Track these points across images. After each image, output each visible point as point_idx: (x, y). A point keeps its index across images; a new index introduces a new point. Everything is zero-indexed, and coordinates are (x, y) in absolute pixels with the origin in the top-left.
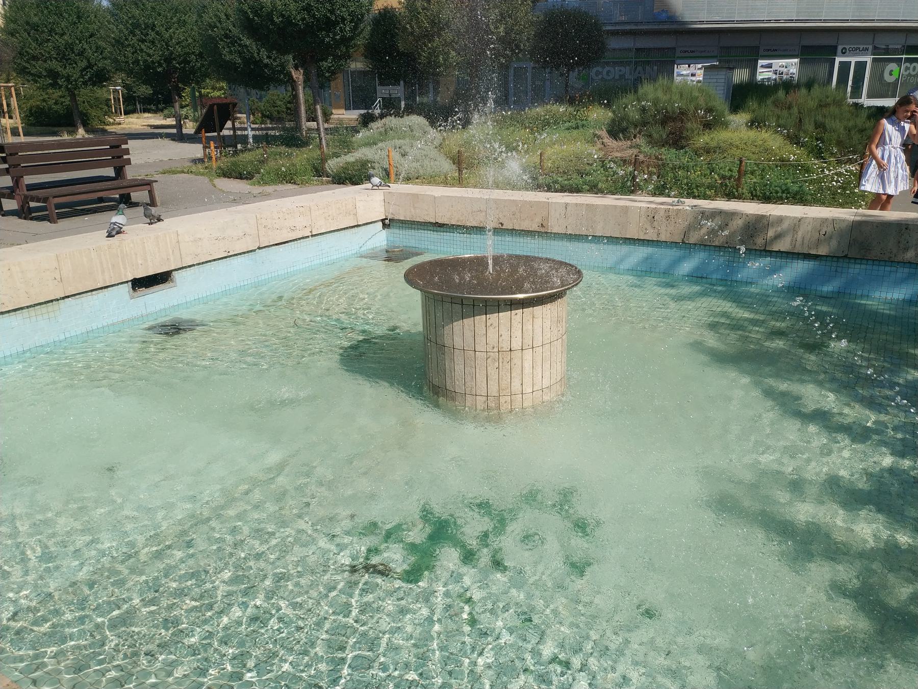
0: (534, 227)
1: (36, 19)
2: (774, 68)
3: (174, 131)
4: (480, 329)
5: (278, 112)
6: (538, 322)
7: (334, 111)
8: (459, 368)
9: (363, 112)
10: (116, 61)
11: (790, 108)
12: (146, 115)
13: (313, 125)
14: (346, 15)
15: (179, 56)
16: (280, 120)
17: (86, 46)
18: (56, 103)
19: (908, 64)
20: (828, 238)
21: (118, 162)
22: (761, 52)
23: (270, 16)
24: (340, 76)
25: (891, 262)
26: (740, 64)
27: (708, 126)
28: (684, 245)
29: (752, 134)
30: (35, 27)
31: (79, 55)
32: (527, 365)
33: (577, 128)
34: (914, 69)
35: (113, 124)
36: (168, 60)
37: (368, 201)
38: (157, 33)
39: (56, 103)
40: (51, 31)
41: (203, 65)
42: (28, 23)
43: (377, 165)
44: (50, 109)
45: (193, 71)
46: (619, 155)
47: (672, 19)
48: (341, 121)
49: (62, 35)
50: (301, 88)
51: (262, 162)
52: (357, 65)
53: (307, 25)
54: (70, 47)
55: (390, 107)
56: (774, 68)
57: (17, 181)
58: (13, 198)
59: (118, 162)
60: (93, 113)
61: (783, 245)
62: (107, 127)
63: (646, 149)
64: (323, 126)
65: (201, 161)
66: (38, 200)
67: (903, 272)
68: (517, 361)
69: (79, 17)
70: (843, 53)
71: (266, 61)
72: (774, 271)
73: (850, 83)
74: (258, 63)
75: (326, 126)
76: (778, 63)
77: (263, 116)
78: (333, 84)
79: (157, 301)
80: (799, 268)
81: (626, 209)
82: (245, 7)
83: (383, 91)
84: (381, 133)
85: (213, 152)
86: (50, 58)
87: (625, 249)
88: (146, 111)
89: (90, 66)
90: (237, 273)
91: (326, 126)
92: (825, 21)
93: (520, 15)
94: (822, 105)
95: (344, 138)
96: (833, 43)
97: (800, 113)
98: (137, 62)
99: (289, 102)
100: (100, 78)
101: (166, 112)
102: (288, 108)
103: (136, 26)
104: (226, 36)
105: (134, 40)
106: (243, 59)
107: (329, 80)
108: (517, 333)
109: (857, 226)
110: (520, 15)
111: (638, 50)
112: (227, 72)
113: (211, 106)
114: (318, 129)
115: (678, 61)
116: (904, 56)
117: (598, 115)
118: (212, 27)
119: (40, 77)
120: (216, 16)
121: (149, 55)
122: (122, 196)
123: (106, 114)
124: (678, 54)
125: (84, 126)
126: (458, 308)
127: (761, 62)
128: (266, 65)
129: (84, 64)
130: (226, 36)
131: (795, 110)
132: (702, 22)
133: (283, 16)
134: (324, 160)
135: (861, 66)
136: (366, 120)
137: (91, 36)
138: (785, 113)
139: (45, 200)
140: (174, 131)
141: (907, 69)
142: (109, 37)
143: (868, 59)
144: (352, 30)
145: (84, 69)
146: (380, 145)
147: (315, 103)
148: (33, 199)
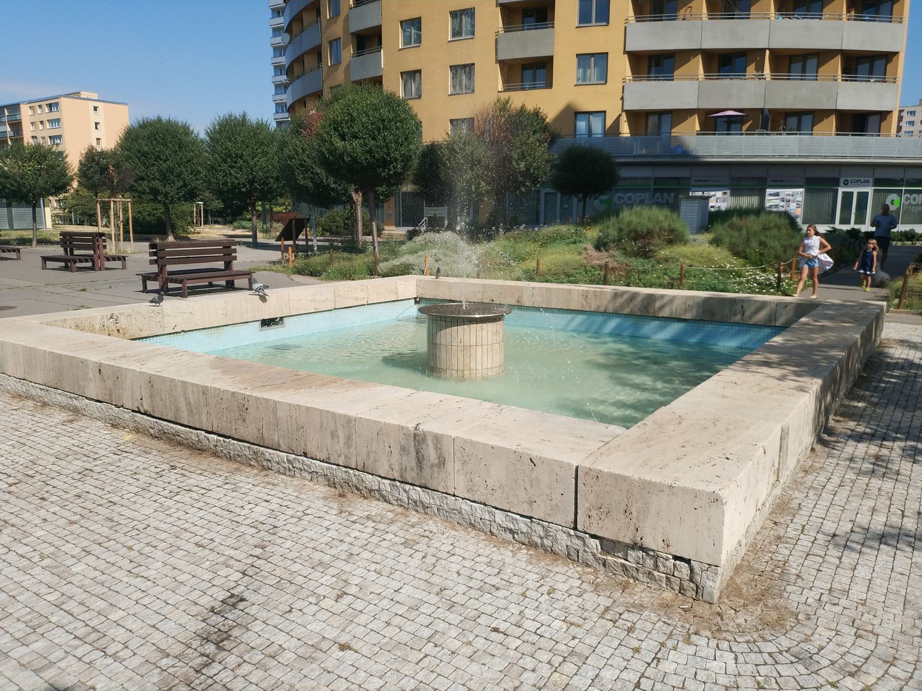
2: (781, 196)
3: (250, 240)
4: (454, 334)
5: (337, 227)
6: (485, 332)
7: (386, 228)
8: (443, 355)
9: (410, 228)
10: (209, 182)
12: (217, 226)
13: (369, 238)
14: (398, 157)
15: (260, 179)
17: (183, 170)
18: (149, 215)
19: (908, 195)
20: (690, 308)
21: (228, 258)
22: (769, 182)
23: (341, 156)
24: (392, 199)
25: (727, 323)
26: (749, 192)
27: (671, 242)
28: (607, 314)
29: (712, 249)
30: (145, 155)
31: (176, 176)
32: (479, 354)
33: (575, 243)
34: (914, 199)
35: (194, 233)
36: (251, 182)
37: (408, 286)
38: (244, 161)
39: (149, 215)
40: (158, 158)
41: (278, 187)
42: (139, 151)
43: (416, 268)
44: (144, 219)
45: (270, 191)
46: (598, 262)
47: (686, 153)
48: (391, 235)
49: (165, 161)
51: (328, 264)
52: (408, 188)
53: (369, 163)
55: (435, 225)
56: (781, 196)
57: (162, 269)
58: (156, 280)
59: (228, 258)
60: (179, 223)
61: (666, 313)
62: (189, 236)
63: (621, 259)
64: (377, 240)
65: (280, 262)
66: (176, 281)
67: (735, 329)
68: (473, 352)
69: (180, 147)
70: (846, 184)
71: (333, 186)
72: (661, 328)
73: (854, 210)
75: (379, 240)
76: (785, 192)
77: (324, 229)
78: (386, 205)
79: (273, 334)
80: (676, 327)
81: (570, 291)
82: (324, 149)
83: (429, 212)
84: (422, 245)
85: (290, 255)
86: (154, 179)
87: (568, 317)
88: (216, 222)
89: (185, 185)
90: (322, 323)
91: (379, 240)
92: (825, 157)
93: (538, 154)
94: (765, 229)
95: (392, 248)
96: (835, 175)
97: (748, 234)
98: (226, 183)
99: (347, 219)
100: (191, 196)
101: (236, 224)
102: (345, 224)
104: (301, 165)
105: (225, 167)
106: (315, 183)
107: (383, 201)
108: (490, 360)
109: (707, 300)
110: (538, 154)
111: (656, 179)
113: (291, 221)
114: (373, 242)
116: (904, 188)
117: (593, 233)
118: (291, 158)
119: (144, 194)
120: (295, 149)
121: (236, 178)
122: (227, 282)
123: (189, 224)
124: (693, 183)
125: (173, 233)
126: (443, 323)
127: (769, 191)
128: (333, 189)
129: (181, 183)
130: (301, 165)
131: (744, 232)
133: (351, 156)
134: (376, 262)
135: (863, 197)
136: (411, 235)
137: (188, 162)
138: (736, 234)
139: (181, 282)
140: (250, 240)
141: (907, 199)
142: (206, 163)
143: (870, 190)
144: (403, 168)
145: (180, 188)
146: (420, 253)
147: (372, 220)
148: (172, 281)
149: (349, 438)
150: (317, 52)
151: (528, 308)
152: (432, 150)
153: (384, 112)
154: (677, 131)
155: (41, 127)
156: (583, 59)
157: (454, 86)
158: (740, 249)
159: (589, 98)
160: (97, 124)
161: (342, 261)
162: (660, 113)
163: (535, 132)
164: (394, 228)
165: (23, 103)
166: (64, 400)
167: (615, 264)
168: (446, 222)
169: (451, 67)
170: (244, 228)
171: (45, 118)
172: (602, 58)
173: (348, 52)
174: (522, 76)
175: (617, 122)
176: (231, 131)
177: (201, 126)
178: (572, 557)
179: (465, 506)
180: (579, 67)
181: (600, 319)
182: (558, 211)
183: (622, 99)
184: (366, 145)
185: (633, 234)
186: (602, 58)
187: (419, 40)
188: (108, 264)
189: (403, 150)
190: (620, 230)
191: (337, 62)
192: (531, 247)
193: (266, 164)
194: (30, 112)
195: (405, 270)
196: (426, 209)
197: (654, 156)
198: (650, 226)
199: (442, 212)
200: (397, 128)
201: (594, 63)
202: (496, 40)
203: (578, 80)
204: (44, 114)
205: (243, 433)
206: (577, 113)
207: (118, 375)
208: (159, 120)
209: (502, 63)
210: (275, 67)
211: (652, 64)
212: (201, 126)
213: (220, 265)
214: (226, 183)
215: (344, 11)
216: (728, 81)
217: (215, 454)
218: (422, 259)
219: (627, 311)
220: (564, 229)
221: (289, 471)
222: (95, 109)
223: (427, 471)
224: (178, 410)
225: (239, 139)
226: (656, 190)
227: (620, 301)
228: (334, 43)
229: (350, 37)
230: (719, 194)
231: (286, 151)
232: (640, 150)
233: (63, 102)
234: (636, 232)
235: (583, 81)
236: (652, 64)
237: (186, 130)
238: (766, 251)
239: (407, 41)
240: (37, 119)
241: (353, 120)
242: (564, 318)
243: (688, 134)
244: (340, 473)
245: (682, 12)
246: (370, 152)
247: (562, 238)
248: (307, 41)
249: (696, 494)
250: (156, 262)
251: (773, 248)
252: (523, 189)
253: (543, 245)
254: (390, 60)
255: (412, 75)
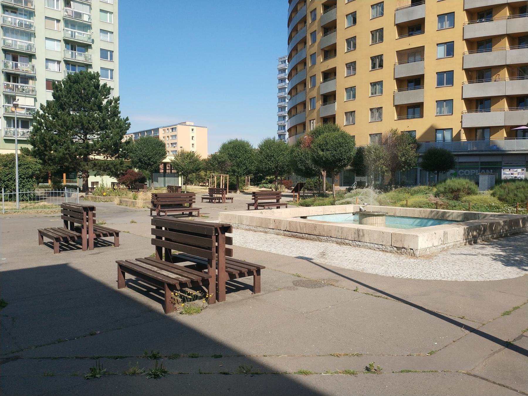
0: (392, 215)
1: (232, 153)
5: (311, 187)
9: (348, 187)
11: (504, 189)
16: (311, 190)
23: (322, 158)
27: (469, 194)
36: (276, 167)
40: (236, 157)
47: (498, 149)
50: (325, 178)
51: (313, 202)
52: (349, 167)
54: (241, 162)
55: (361, 185)
57: (256, 201)
61: (450, 218)
66: (261, 206)
74: (311, 170)
82: (314, 155)
83: (357, 179)
89: (246, 168)
98: (266, 168)
103: (268, 156)
105: (266, 160)
111: (482, 162)
112: (299, 172)
115: (503, 168)
117: (435, 190)
118: (296, 157)
124: (503, 164)
129: (245, 168)
131: (507, 190)
132: (514, 151)
134: (334, 201)
136: (349, 190)
138: (503, 190)
139: (263, 206)
149: (342, 232)
150: (304, 104)
151: (398, 217)
152: (360, 151)
153: (340, 140)
154: (493, 138)
155: (167, 139)
156: (439, 103)
157: (372, 117)
158: (504, 197)
159: (442, 122)
160: (193, 137)
161: (319, 200)
162: (483, 128)
163: (409, 144)
164: (339, 187)
165: (161, 127)
166: (262, 230)
167: (442, 203)
168: (367, 184)
169: (371, 83)
170: (265, 187)
171: (169, 135)
172: (450, 102)
173: (319, 103)
174: (407, 112)
175: (459, 134)
176: (268, 145)
177: (255, 144)
178: (391, 252)
179: (369, 244)
180: (437, 107)
181: (426, 221)
182: (427, 179)
183: (461, 122)
184: (332, 153)
185: (451, 190)
186: (450, 102)
187: (354, 97)
188: (227, 201)
189: (348, 155)
190: (445, 188)
191: (314, 108)
192: (407, 195)
193: (283, 159)
194: (163, 132)
195: (348, 203)
196: (356, 178)
197: (480, 151)
198: (459, 187)
199: (364, 179)
200: (346, 146)
201: (445, 105)
202: (394, 96)
203: (437, 113)
204: (170, 133)
205: (315, 233)
206: (437, 130)
207: (280, 222)
208: (237, 140)
209: (397, 106)
210: (279, 108)
211: (477, 104)
212: (255, 144)
213: (275, 201)
214: (266, 168)
215: (318, 84)
216: (522, 111)
217: (307, 239)
218: (355, 200)
219: (436, 218)
220: (422, 187)
221: (327, 241)
222: (192, 130)
223: (360, 238)
224: (297, 229)
225: (272, 148)
226: (482, 168)
227: (433, 214)
228: (312, 99)
229: (320, 97)
230: (519, 170)
231: (294, 154)
232: (472, 148)
233: (179, 127)
234: (452, 189)
235: (440, 114)
236: (477, 104)
237: (248, 144)
238: (516, 198)
239: (349, 97)
240: (166, 135)
241: (327, 143)
242: (412, 221)
243: (500, 140)
244: (340, 240)
245: (494, 77)
246: (334, 156)
247: (422, 192)
248: (299, 99)
249: (413, 235)
250: (254, 199)
251: (520, 197)
252: (404, 169)
253: (412, 195)
254: (339, 108)
255: (350, 114)
